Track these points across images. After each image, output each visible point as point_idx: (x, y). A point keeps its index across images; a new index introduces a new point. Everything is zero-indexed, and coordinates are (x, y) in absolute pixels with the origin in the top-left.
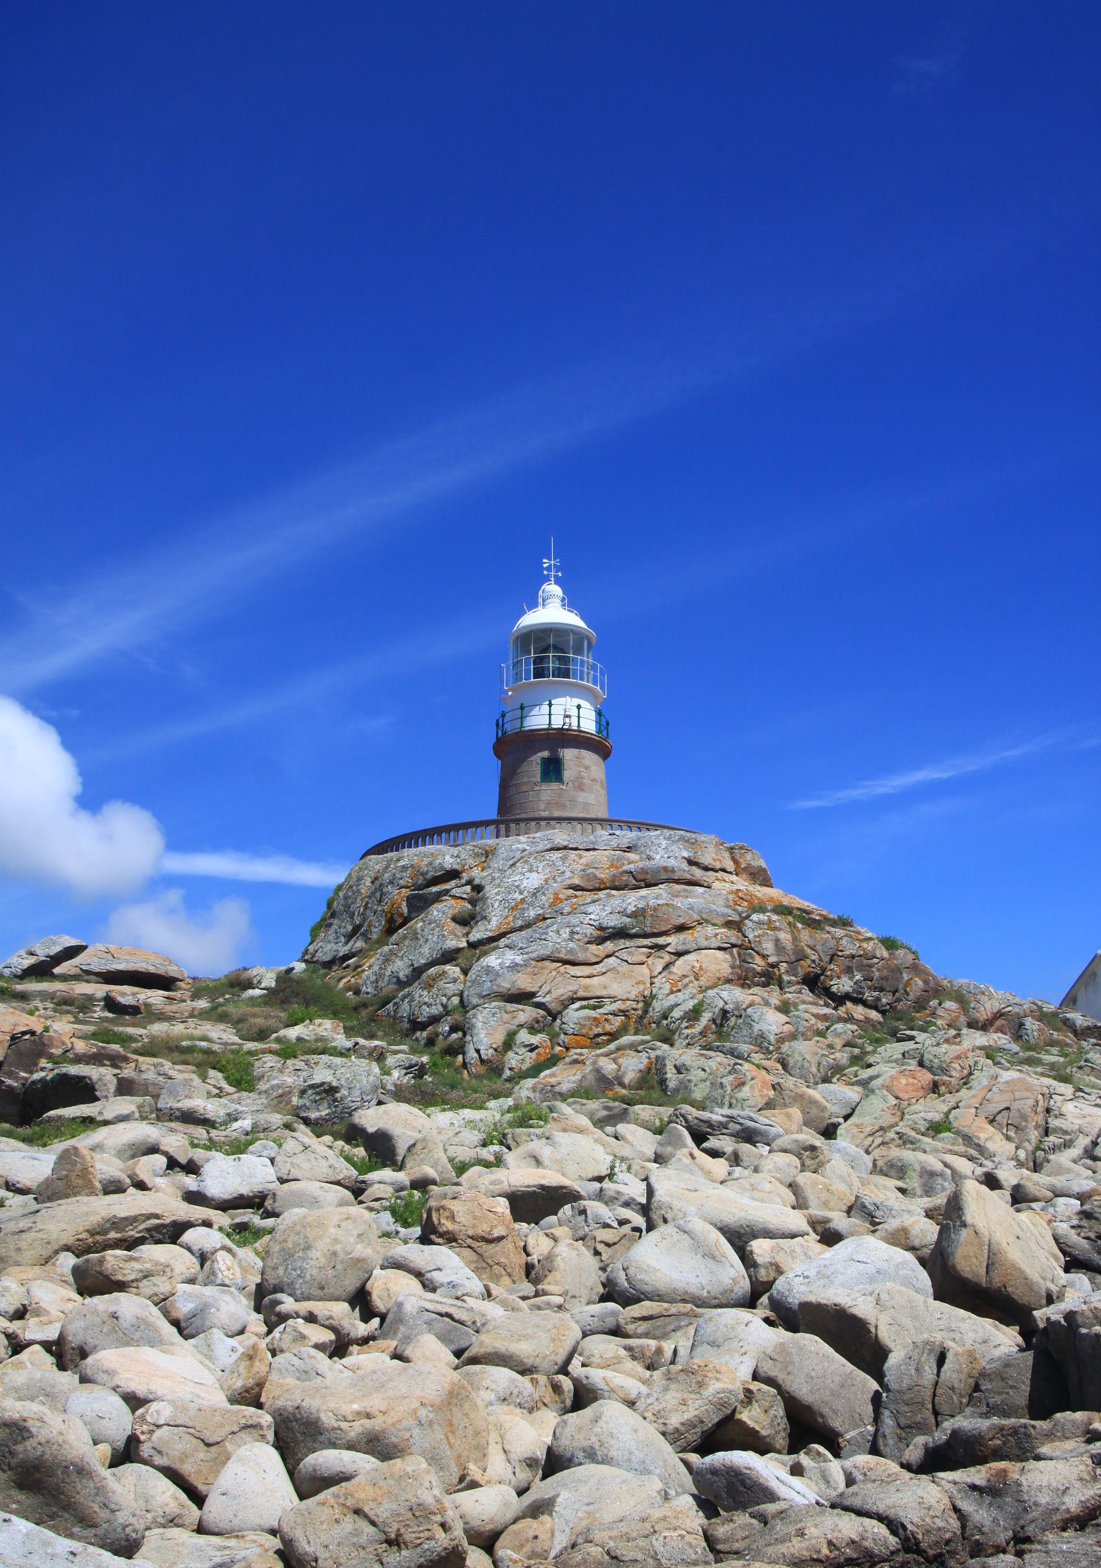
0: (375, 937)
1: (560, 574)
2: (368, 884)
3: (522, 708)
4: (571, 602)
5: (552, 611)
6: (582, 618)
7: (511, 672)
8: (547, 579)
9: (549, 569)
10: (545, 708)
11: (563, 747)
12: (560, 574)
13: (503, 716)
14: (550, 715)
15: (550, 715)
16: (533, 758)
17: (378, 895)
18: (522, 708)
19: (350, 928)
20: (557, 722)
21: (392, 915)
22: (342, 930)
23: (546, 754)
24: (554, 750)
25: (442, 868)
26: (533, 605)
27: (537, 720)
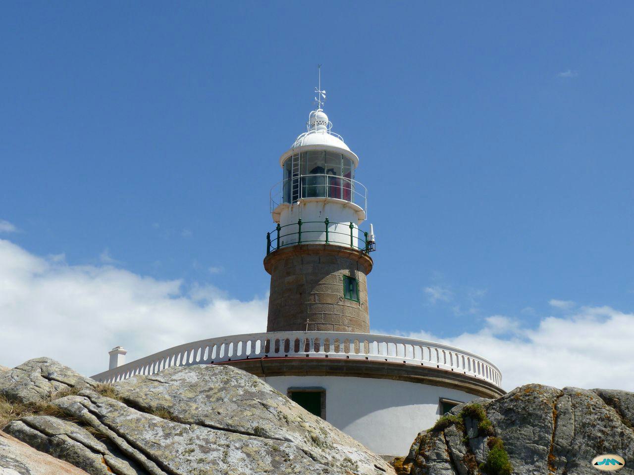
3: (300, 223)
6: (350, 149)
16: (335, 273)
17: (528, 394)
18: (300, 223)
23: (347, 272)
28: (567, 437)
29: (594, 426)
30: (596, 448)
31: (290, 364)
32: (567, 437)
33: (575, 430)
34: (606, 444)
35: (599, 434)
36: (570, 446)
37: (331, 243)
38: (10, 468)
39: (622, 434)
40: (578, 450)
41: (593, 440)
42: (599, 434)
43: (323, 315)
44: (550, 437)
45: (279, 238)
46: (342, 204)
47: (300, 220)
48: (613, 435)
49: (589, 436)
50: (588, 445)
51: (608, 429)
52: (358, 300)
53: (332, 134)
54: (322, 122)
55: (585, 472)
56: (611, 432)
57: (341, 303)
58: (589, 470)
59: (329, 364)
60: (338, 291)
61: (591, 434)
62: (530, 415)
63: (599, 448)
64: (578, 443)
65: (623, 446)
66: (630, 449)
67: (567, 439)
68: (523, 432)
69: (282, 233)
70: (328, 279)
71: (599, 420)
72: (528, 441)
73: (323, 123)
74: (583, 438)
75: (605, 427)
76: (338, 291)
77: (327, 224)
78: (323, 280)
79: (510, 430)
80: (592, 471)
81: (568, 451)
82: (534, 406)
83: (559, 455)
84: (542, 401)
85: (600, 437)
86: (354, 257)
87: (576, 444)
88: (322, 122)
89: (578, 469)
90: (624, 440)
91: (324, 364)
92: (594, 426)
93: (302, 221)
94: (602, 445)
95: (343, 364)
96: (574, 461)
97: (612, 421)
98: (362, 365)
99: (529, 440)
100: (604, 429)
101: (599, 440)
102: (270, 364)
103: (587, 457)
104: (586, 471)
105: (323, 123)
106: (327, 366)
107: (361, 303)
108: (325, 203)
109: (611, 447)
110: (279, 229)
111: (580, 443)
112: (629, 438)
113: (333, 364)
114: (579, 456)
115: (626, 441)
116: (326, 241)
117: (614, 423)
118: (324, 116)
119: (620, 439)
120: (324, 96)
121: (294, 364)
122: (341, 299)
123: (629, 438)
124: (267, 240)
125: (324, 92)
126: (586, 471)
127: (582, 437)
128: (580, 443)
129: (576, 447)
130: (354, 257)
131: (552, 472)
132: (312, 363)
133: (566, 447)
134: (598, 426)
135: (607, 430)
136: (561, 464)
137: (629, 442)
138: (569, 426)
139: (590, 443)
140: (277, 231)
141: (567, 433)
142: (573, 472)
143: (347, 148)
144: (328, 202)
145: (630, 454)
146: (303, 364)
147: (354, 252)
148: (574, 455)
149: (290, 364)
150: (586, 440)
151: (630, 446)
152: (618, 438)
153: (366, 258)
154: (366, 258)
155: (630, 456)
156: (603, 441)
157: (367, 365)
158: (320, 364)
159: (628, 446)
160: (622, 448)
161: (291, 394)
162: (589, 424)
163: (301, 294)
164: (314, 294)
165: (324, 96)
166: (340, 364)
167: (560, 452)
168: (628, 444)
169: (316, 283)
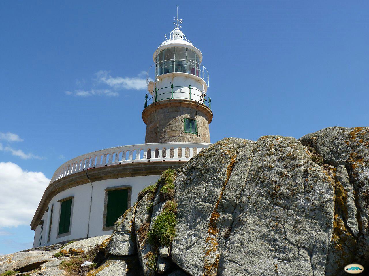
3: (156, 91)
4: (187, 36)
5: (178, 39)
14: (190, 94)
15: (190, 94)
18: (172, 87)
23: (187, 116)
27: (182, 94)
28: (236, 188)
29: (271, 169)
30: (269, 198)
31: (105, 170)
32: (236, 188)
33: (248, 178)
34: (284, 189)
35: (276, 178)
36: (239, 198)
37: (174, 99)
38: (79, 255)
39: (306, 173)
40: (246, 202)
41: (267, 186)
42: (276, 178)
44: (218, 191)
46: (185, 76)
48: (294, 177)
49: (262, 183)
50: (259, 194)
51: (290, 169)
52: (197, 133)
53: (187, 41)
54: (178, 35)
55: (251, 231)
56: (292, 173)
57: (182, 135)
58: (257, 227)
59: (132, 167)
60: (180, 128)
61: (265, 179)
62: (207, 169)
63: (273, 196)
64: (248, 194)
65: (306, 190)
66: (315, 192)
67: (235, 190)
68: (197, 191)
70: (174, 121)
71: (279, 161)
72: (198, 200)
74: (256, 186)
75: (285, 167)
76: (180, 128)
77: (172, 88)
78: (170, 122)
79: (187, 190)
80: (261, 229)
81: (236, 205)
82: (213, 159)
83: (225, 212)
84: (222, 153)
85: (276, 182)
86: (192, 106)
87: (246, 195)
88: (178, 35)
89: (243, 227)
90: (308, 181)
91: (128, 167)
92: (271, 169)
94: (277, 192)
95: (143, 166)
96: (240, 218)
97: (295, 159)
98: (157, 165)
99: (199, 199)
100: (283, 170)
101: (274, 186)
102: (92, 173)
103: (257, 210)
104: (253, 230)
105: (180, 36)
106: (130, 169)
107: (199, 135)
108: (174, 77)
109: (290, 193)
111: (251, 193)
112: (315, 177)
113: (135, 167)
114: (247, 210)
115: (310, 182)
117: (297, 161)
118: (181, 33)
119: (302, 181)
120: (182, 22)
121: (107, 170)
122: (182, 133)
123: (315, 177)
125: (181, 20)
126: (253, 230)
127: (254, 184)
128: (251, 193)
129: (245, 199)
130: (192, 106)
131: (212, 236)
132: (119, 168)
133: (233, 200)
134: (276, 168)
135: (288, 172)
136: (224, 223)
137: (315, 183)
138: (242, 174)
139: (262, 191)
141: (237, 183)
142: (236, 233)
143: (192, 45)
144: (175, 76)
145: (315, 199)
146: (113, 169)
147: (191, 103)
148: (242, 210)
149: (105, 170)
150: (258, 187)
151: (316, 188)
152: (300, 180)
153: (202, 106)
154: (202, 106)
155: (315, 202)
156: (280, 186)
157: (161, 165)
158: (125, 168)
159: (312, 188)
160: (304, 192)
161: (107, 193)
162: (265, 167)
163: (157, 133)
164: (164, 132)
165: (182, 22)
166: (140, 166)
167: (226, 208)
168: (312, 186)
169: (165, 125)
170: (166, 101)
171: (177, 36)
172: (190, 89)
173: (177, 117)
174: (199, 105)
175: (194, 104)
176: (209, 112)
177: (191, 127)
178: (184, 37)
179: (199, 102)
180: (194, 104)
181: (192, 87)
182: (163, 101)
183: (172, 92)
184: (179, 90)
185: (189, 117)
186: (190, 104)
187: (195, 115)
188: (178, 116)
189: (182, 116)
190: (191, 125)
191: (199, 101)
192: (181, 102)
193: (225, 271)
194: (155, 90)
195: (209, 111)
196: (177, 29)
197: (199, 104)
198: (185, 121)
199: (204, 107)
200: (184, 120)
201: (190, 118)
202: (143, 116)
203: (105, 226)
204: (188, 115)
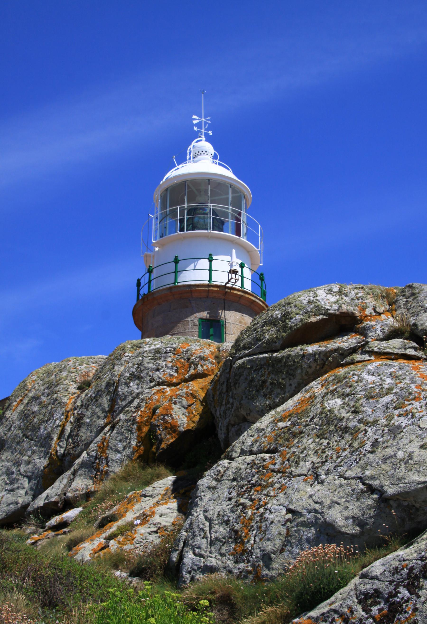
0: (116, 469)
1: (210, 133)
2: (73, 388)
3: (176, 261)
4: (223, 156)
5: (203, 162)
6: (234, 173)
7: (158, 225)
8: (196, 135)
9: (199, 125)
10: (204, 263)
11: (225, 309)
12: (210, 133)
13: (150, 271)
14: (210, 270)
15: (210, 270)
16: (189, 319)
17: (105, 401)
18: (176, 261)
19: (42, 463)
20: (220, 278)
21: (153, 428)
22: (23, 469)
23: (204, 314)
24: (213, 311)
25: (318, 309)
26: (182, 159)
27: (196, 274)
37: (179, 284)
43: (324, 418)
45: (150, 282)
47: (176, 257)
53: (219, 164)
54: (201, 152)
69: (154, 275)
73: (202, 153)
88: (201, 152)
93: (179, 259)
105: (202, 153)
110: (150, 271)
116: (209, 281)
118: (209, 147)
124: (136, 288)
140: (148, 274)
153: (236, 292)
154: (236, 292)
170: (165, 289)
171: (199, 154)
172: (211, 261)
173: (186, 319)
174: (229, 291)
175: (216, 289)
176: (254, 301)
177: (212, 335)
178: (215, 157)
179: (228, 285)
180: (216, 289)
181: (214, 257)
182: (159, 290)
183: (175, 272)
184: (192, 267)
185: (208, 315)
186: (209, 290)
187: (220, 311)
188: (187, 317)
189: (195, 315)
190: (212, 331)
191: (226, 283)
192: (191, 289)
193: (336, 508)
194: (149, 269)
195: (253, 298)
196: (201, 140)
197: (228, 288)
198: (200, 324)
199: (239, 293)
200: (197, 323)
201: (210, 316)
202: (136, 324)
203: (170, 492)
204: (207, 312)
